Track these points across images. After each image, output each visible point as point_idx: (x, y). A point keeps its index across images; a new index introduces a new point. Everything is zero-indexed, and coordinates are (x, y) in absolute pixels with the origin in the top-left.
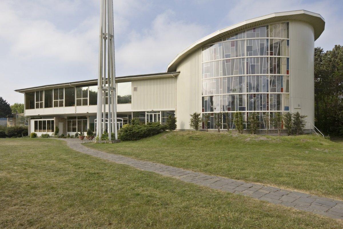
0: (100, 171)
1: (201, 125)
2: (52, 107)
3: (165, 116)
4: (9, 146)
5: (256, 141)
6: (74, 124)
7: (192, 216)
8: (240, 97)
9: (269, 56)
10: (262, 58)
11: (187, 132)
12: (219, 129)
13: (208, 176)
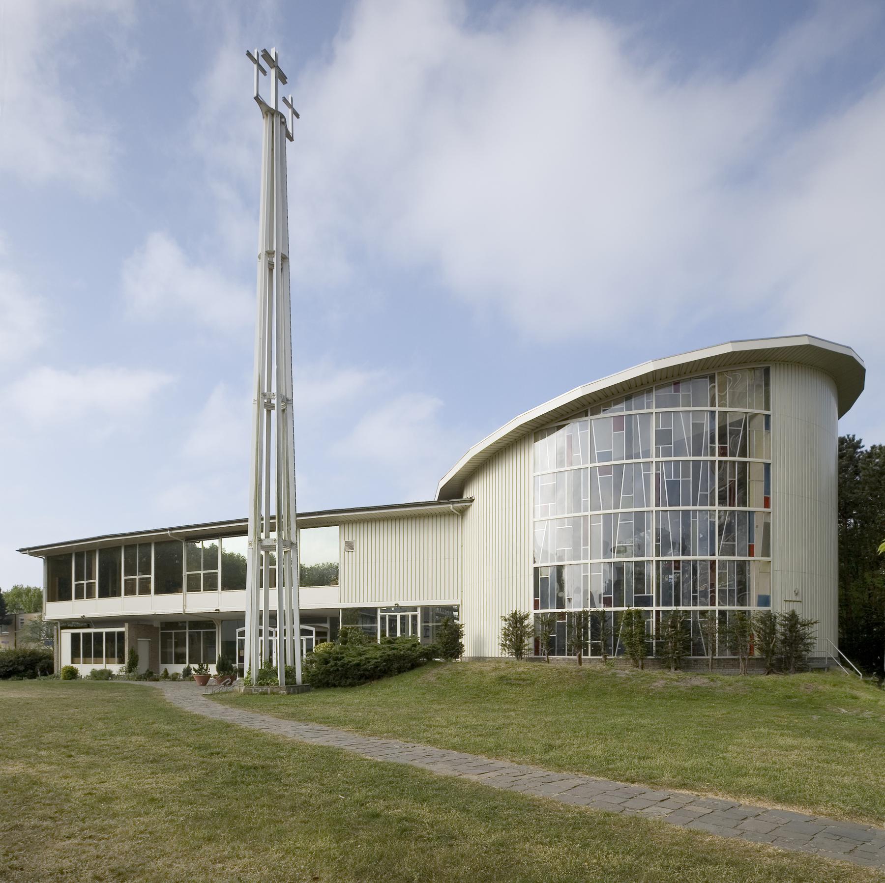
0: (268, 762)
1: (532, 646)
2: (120, 595)
3: (431, 620)
4: (11, 700)
5: (682, 689)
6: (180, 643)
7: (518, 862)
8: (638, 569)
9: (717, 458)
10: (696, 463)
11: (493, 665)
12: (580, 656)
13: (553, 774)
